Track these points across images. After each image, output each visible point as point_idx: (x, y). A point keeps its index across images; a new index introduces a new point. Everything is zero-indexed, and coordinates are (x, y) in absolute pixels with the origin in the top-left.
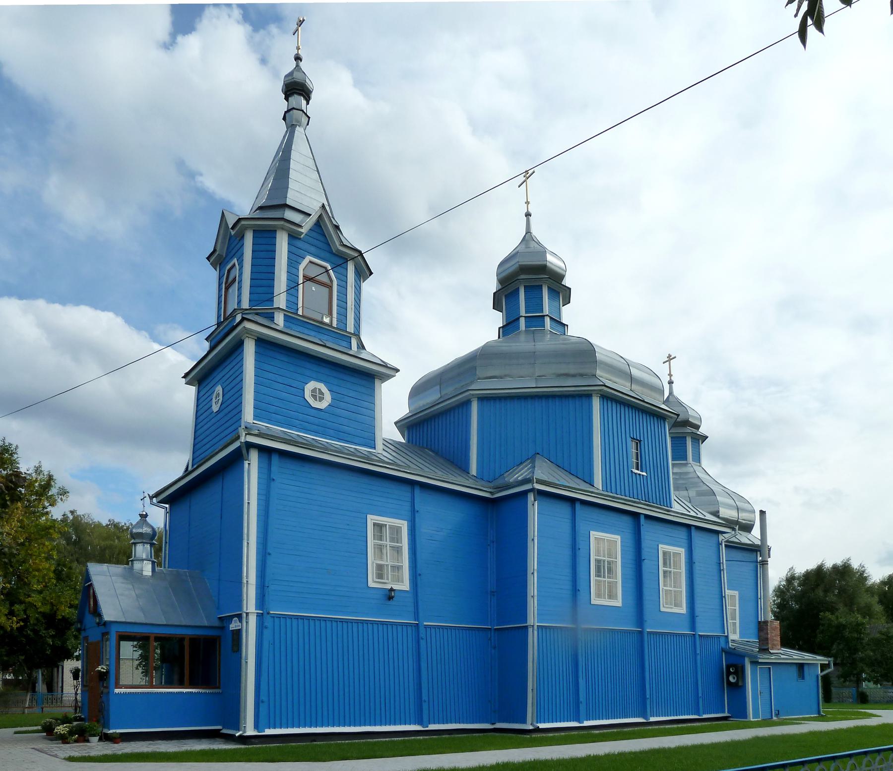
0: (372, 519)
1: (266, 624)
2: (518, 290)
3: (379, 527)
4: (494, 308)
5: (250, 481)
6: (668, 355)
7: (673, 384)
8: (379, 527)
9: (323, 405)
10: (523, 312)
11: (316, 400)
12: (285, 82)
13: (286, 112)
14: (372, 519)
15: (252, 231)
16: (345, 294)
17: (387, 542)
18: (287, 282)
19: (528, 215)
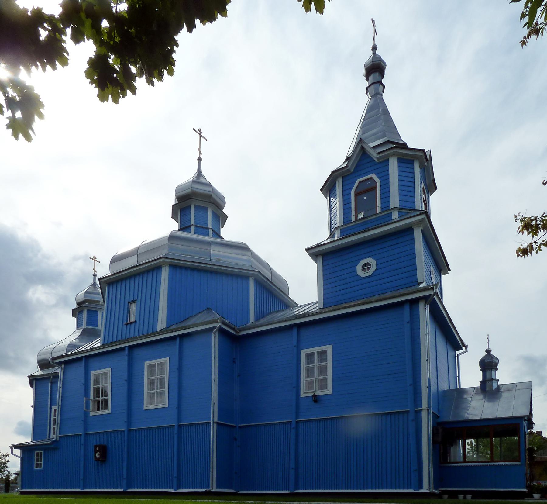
0: (329, 348)
1: (409, 325)
2: (189, 207)
3: (323, 354)
4: (227, 217)
5: (376, 83)
6: (96, 257)
7: (96, 277)
8: (323, 354)
9: (359, 268)
10: (193, 222)
11: (362, 267)
12: (366, 68)
13: (367, 88)
14: (329, 348)
15: (398, 212)
16: (414, 202)
17: (316, 364)
18: (399, 202)
19: (200, 159)
